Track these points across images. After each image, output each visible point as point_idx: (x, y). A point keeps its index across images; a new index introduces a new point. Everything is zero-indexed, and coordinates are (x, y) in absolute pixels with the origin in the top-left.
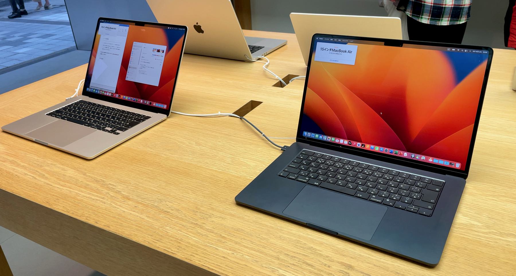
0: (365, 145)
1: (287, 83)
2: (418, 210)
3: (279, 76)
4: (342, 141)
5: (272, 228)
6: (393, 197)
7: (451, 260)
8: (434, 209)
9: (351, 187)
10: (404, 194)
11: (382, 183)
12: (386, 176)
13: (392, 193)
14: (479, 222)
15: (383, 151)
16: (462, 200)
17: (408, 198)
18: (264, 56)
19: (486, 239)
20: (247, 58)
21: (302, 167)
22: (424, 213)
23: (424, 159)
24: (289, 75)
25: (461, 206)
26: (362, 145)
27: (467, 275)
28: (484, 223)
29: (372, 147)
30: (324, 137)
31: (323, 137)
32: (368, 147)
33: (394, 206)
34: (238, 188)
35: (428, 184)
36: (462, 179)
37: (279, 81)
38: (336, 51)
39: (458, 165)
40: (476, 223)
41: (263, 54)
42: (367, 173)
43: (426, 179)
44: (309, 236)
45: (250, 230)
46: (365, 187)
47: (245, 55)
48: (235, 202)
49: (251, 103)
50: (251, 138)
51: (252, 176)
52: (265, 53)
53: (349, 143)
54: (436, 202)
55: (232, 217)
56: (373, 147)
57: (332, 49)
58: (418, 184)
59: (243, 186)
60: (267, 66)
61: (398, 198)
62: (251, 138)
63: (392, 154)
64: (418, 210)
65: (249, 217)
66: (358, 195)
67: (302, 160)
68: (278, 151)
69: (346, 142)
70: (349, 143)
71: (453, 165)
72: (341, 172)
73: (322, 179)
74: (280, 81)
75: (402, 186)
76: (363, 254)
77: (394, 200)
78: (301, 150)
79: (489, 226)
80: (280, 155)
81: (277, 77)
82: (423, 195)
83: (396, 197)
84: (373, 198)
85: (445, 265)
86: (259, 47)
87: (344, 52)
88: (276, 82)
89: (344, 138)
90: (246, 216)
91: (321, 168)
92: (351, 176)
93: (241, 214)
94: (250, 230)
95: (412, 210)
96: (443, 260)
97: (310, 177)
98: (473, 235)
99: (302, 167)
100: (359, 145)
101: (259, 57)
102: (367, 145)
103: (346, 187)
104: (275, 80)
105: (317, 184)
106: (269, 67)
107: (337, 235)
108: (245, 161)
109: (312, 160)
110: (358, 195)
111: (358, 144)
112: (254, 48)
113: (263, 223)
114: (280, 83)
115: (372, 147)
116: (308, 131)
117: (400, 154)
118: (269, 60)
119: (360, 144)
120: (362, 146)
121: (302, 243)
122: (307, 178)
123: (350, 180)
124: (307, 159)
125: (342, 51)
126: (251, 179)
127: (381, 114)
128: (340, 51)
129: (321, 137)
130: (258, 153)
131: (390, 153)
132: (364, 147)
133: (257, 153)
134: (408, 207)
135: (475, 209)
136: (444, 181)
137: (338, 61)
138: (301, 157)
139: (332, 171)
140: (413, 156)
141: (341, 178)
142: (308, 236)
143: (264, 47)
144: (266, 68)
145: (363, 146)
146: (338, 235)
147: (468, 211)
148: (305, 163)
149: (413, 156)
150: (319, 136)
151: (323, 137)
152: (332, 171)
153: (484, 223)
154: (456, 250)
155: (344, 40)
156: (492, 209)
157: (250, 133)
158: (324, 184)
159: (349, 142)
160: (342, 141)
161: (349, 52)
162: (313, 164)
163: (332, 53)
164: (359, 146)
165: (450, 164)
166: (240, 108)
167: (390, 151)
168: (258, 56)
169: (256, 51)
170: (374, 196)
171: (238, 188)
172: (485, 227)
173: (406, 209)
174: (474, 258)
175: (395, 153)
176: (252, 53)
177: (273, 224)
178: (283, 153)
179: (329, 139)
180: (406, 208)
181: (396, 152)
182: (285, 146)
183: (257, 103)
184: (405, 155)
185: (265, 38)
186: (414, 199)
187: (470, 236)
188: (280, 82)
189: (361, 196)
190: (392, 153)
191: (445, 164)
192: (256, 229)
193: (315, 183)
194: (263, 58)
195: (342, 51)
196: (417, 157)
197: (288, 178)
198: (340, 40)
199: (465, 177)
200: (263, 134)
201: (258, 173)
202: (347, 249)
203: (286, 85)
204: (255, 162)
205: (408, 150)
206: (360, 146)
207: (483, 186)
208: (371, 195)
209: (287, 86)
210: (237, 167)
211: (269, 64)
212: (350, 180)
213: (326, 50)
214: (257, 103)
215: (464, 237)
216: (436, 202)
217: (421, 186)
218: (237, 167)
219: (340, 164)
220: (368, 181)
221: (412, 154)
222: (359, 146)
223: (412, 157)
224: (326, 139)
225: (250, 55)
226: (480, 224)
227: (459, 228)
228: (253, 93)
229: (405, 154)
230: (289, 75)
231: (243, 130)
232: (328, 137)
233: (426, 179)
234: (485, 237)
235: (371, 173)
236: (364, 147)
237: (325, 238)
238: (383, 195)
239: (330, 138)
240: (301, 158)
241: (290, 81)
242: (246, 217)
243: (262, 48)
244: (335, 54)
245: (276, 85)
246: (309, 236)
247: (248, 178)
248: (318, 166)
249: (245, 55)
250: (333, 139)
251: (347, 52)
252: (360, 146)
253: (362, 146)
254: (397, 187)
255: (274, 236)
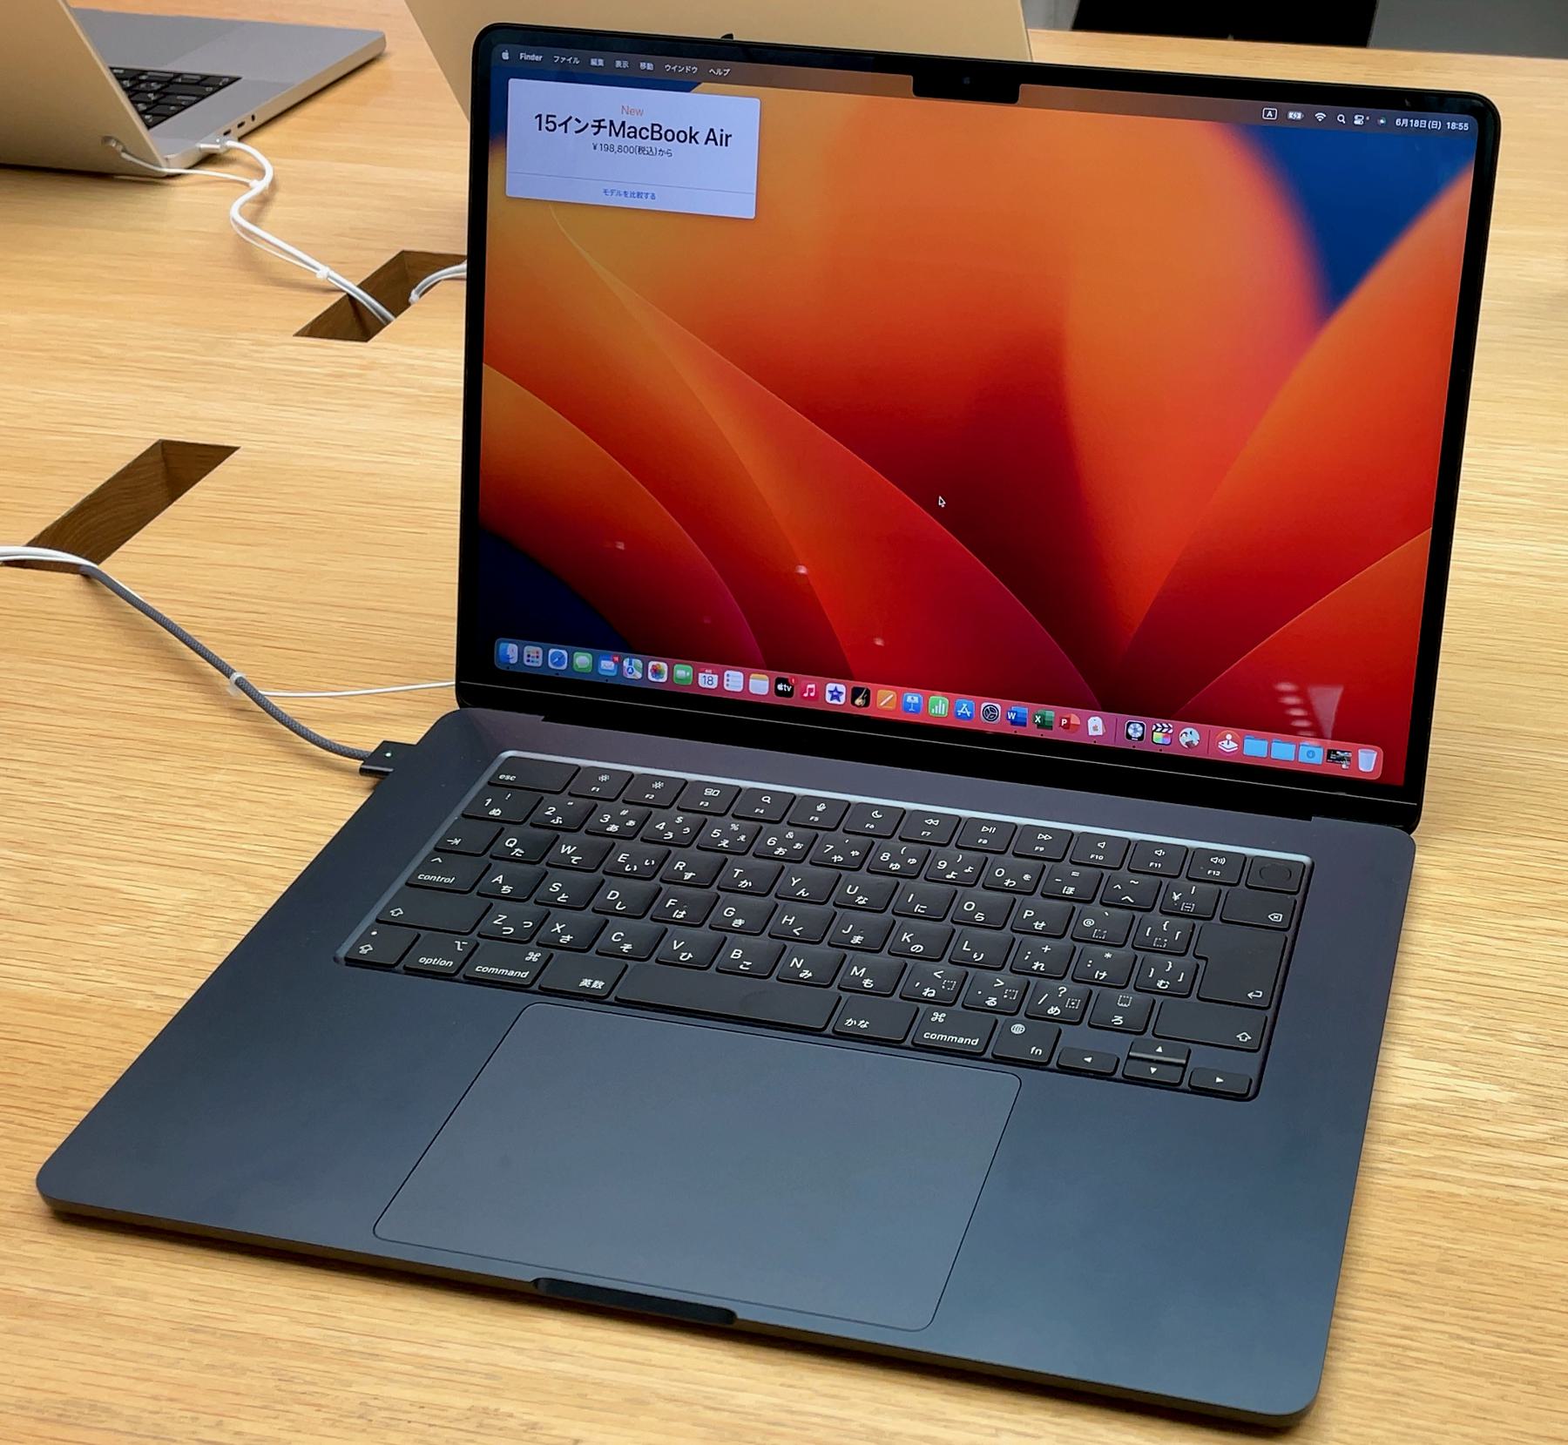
0: (868, 692)
1: (399, 305)
2: (1185, 1066)
3: (337, 265)
4: (734, 681)
5: (306, 1349)
6: (1047, 1004)
7: (1378, 1358)
8: (1264, 1044)
9: (806, 974)
10: (1104, 974)
11: (980, 917)
12: (999, 873)
13: (1037, 974)
14: (1496, 1079)
15: (969, 718)
16: (1407, 959)
17: (1126, 999)
18: (240, 139)
19: (1545, 1184)
20: (124, 155)
21: (500, 879)
22: (1218, 1080)
23: (1196, 743)
24: (403, 255)
25: (1398, 997)
26: (855, 693)
27: (1465, 1436)
28: (1522, 1081)
29: (913, 698)
30: (626, 663)
31: (619, 665)
32: (886, 700)
33: (1053, 1065)
34: (65, 1091)
35: (1225, 889)
36: (1393, 832)
37: (341, 295)
38: (635, 133)
39: (1367, 761)
40: (1483, 1091)
41: (232, 125)
42: (896, 866)
43: (1215, 860)
44: (558, 1366)
45: (155, 1398)
46: (883, 958)
47: (107, 139)
48: (38, 1202)
49: (159, 457)
50: (160, 707)
51: (164, 982)
52: (246, 117)
53: (780, 687)
54: (1275, 999)
55: (23, 1322)
56: (916, 700)
57: (607, 123)
58: (1176, 897)
59: (103, 1068)
60: (264, 200)
61: (1075, 1004)
62: (160, 707)
63: (1021, 731)
64: (1185, 1066)
65: (144, 1296)
66: (850, 1022)
67: (496, 827)
68: (337, 777)
69: (760, 685)
70: (780, 687)
71: (1342, 759)
72: (744, 884)
73: (626, 947)
74: (348, 295)
75: (1089, 923)
76: (888, 1424)
77: (1052, 1019)
78: (491, 762)
79: (1550, 1097)
80: (356, 809)
81: (323, 272)
82: (1202, 963)
83: (1059, 998)
84: (937, 1027)
85: (1351, 1397)
86: (205, 77)
87: (682, 137)
88: (319, 306)
89: (746, 662)
90: (122, 1292)
91: (618, 872)
92: (801, 900)
93: (90, 1288)
94: (155, 1398)
95: (1153, 1070)
96: (1342, 1364)
97: (551, 944)
98: (1476, 1167)
99: (500, 879)
100: (835, 693)
101: (203, 146)
102: (881, 692)
103: (773, 978)
104: (314, 295)
105: (598, 984)
106: (274, 212)
107: (730, 1326)
108: (114, 884)
109: (558, 820)
110: (850, 1022)
111: (830, 687)
112: (171, 89)
113: (250, 1323)
114: (351, 310)
115: (909, 699)
116: (525, 635)
117: (1067, 726)
118: (272, 164)
119: (842, 688)
120: (854, 697)
121: (512, 1423)
122: (533, 957)
123: (795, 925)
124: (527, 818)
125: (670, 135)
126: (156, 1006)
127: (942, 504)
128: (656, 132)
129: (607, 666)
130: (209, 814)
131: (1013, 723)
132: (867, 704)
133: (198, 811)
134: (1130, 1057)
135: (1465, 1006)
136: (1305, 859)
137: (653, 197)
138: (491, 807)
139: (688, 884)
140: (1135, 730)
141: (740, 922)
142: (553, 1366)
143: (234, 80)
144: (254, 221)
145: (858, 701)
146: (735, 1324)
147: (1439, 1025)
148: (518, 852)
149: (1135, 730)
150: (595, 663)
151: (619, 665)
152: (688, 884)
153: (1522, 1081)
154: (1397, 1285)
155: (672, 66)
156: (1554, 991)
157: (156, 675)
158: (643, 982)
159: (779, 681)
160: (734, 681)
161: (711, 137)
162: (569, 850)
163: (610, 148)
164: (835, 702)
165: (1328, 757)
166: (84, 501)
167: (1012, 716)
168: (199, 139)
169: (186, 107)
170: (939, 1017)
171: (65, 1091)
172: (1531, 1111)
173: (1118, 1075)
174: (1490, 1317)
175: (1039, 726)
176: (149, 127)
177: (313, 1319)
178: (375, 788)
179: (656, 672)
180: (1121, 1064)
181: (1043, 718)
182: (386, 745)
183: (209, 457)
184: (1095, 728)
185: (242, 23)
186: (1159, 999)
187: (1460, 1181)
188: (347, 298)
189: (863, 1024)
190: (1025, 725)
191: (1303, 758)
192: (194, 1386)
193: (586, 982)
194: (229, 149)
195: (670, 135)
196: (1158, 737)
197: (410, 971)
198: (650, 66)
199: (1408, 818)
200: (236, 676)
201: (269, 884)
202: (796, 1407)
203: (388, 322)
204: (187, 875)
205: (1105, 704)
206: (843, 698)
207: (1499, 857)
208: (923, 1007)
209: (398, 324)
210: (60, 931)
211: (273, 185)
212: (795, 925)
213: (573, 125)
214: (209, 457)
215: (1431, 1195)
216: (1275, 999)
217: (1190, 907)
218: (60, 931)
219: (735, 827)
220: (899, 920)
221: (1129, 718)
222: (835, 702)
223: (1129, 737)
224: (639, 675)
225: (142, 138)
226: (1504, 1096)
227: (1404, 1136)
228: (167, 389)
229: (1095, 726)
230: (403, 252)
231: (100, 654)
232: (651, 664)
233: (1215, 860)
234: (1534, 1172)
235: (914, 861)
236: (867, 704)
237: (655, 1357)
238: (992, 1002)
239: (664, 666)
240: (494, 819)
241: (414, 296)
242: (124, 1306)
243: (221, 88)
244: (629, 149)
245: (323, 328)
246: (558, 1366)
247: (141, 1004)
248: (598, 858)
249: (107, 139)
250: (683, 672)
251: (701, 138)
252: (843, 698)
253: (854, 697)
254: (1063, 859)
255: (319, 1407)
